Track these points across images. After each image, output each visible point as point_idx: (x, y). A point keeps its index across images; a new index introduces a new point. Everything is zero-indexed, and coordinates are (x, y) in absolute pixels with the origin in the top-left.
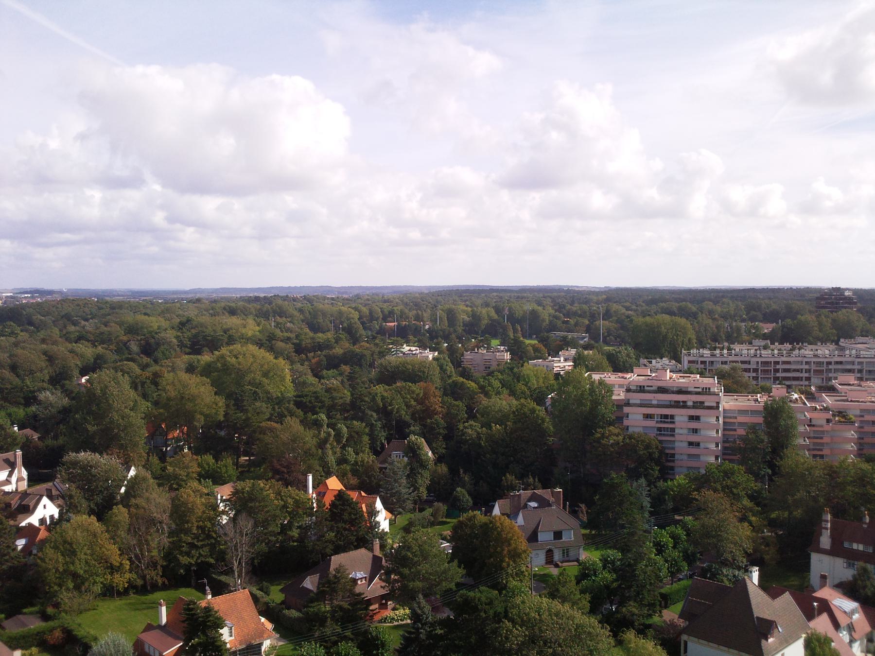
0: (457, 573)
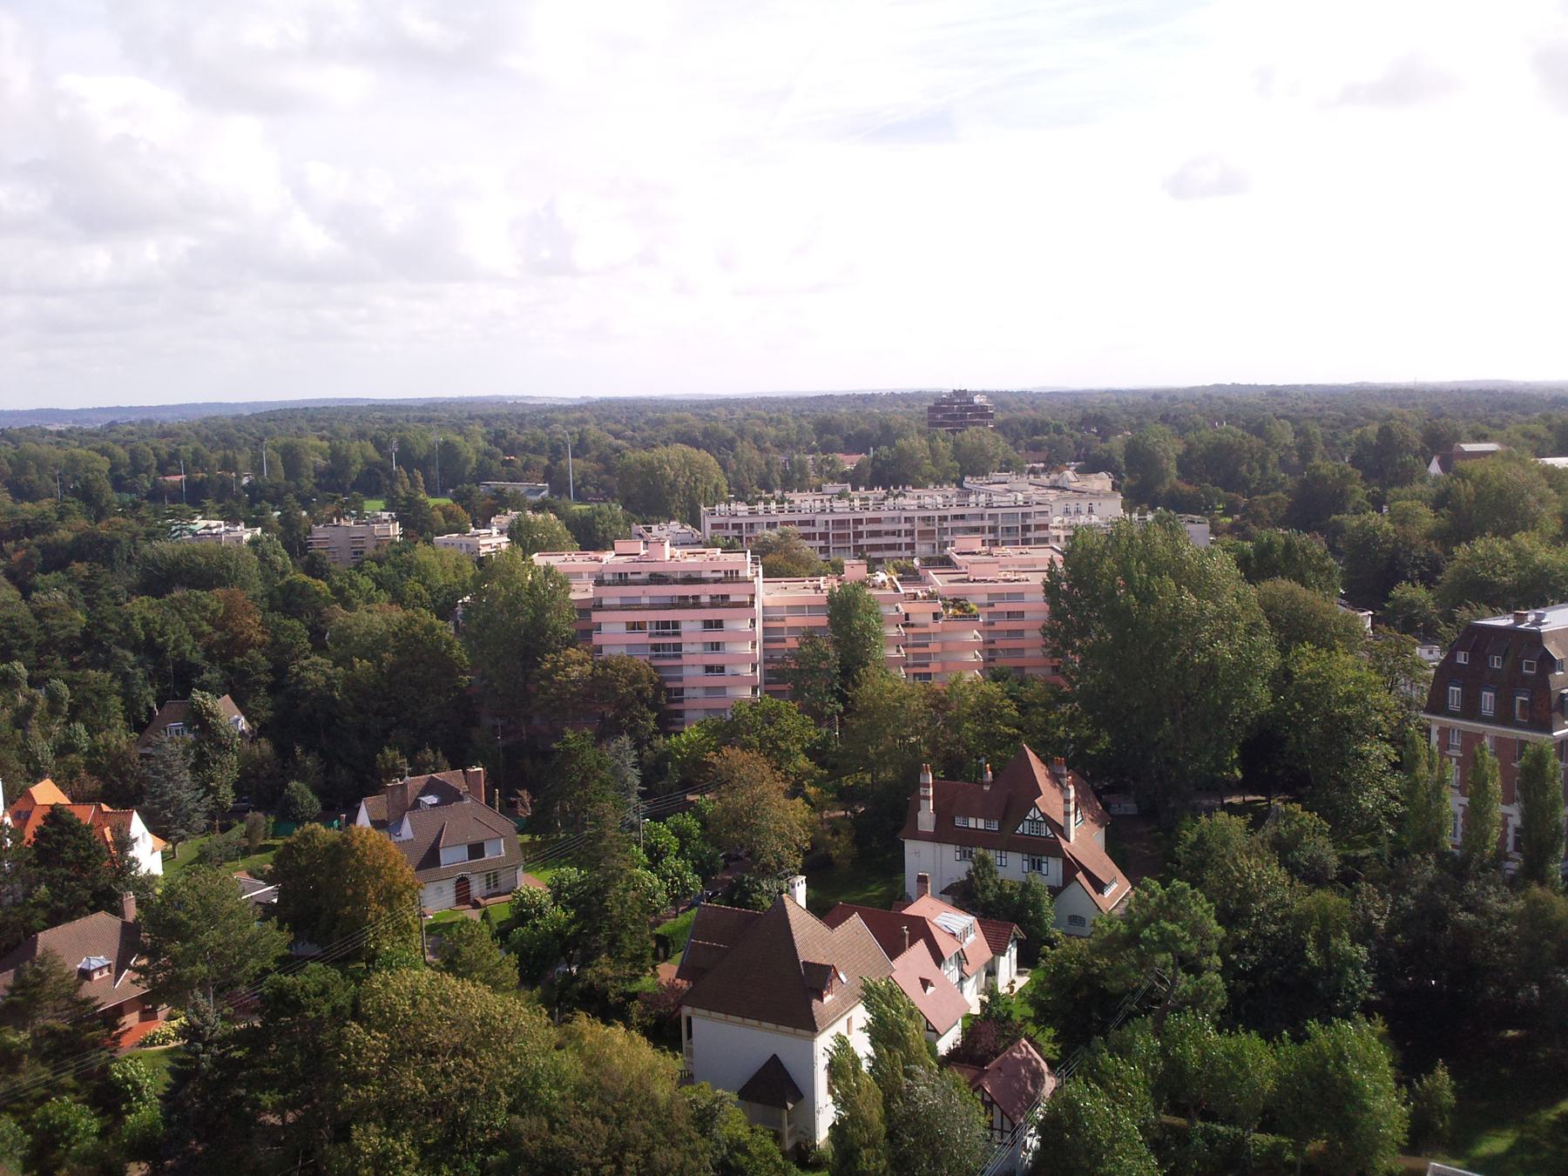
0: (277, 940)
